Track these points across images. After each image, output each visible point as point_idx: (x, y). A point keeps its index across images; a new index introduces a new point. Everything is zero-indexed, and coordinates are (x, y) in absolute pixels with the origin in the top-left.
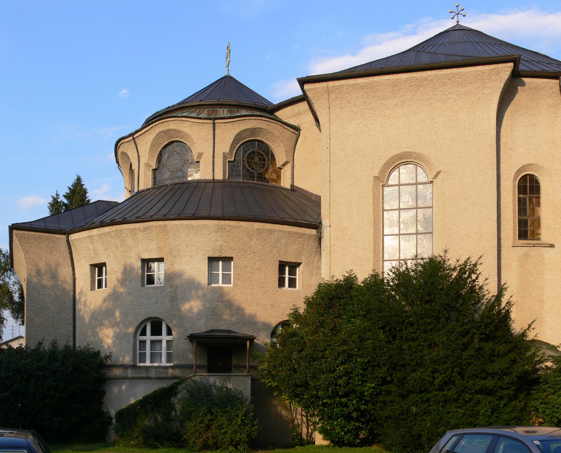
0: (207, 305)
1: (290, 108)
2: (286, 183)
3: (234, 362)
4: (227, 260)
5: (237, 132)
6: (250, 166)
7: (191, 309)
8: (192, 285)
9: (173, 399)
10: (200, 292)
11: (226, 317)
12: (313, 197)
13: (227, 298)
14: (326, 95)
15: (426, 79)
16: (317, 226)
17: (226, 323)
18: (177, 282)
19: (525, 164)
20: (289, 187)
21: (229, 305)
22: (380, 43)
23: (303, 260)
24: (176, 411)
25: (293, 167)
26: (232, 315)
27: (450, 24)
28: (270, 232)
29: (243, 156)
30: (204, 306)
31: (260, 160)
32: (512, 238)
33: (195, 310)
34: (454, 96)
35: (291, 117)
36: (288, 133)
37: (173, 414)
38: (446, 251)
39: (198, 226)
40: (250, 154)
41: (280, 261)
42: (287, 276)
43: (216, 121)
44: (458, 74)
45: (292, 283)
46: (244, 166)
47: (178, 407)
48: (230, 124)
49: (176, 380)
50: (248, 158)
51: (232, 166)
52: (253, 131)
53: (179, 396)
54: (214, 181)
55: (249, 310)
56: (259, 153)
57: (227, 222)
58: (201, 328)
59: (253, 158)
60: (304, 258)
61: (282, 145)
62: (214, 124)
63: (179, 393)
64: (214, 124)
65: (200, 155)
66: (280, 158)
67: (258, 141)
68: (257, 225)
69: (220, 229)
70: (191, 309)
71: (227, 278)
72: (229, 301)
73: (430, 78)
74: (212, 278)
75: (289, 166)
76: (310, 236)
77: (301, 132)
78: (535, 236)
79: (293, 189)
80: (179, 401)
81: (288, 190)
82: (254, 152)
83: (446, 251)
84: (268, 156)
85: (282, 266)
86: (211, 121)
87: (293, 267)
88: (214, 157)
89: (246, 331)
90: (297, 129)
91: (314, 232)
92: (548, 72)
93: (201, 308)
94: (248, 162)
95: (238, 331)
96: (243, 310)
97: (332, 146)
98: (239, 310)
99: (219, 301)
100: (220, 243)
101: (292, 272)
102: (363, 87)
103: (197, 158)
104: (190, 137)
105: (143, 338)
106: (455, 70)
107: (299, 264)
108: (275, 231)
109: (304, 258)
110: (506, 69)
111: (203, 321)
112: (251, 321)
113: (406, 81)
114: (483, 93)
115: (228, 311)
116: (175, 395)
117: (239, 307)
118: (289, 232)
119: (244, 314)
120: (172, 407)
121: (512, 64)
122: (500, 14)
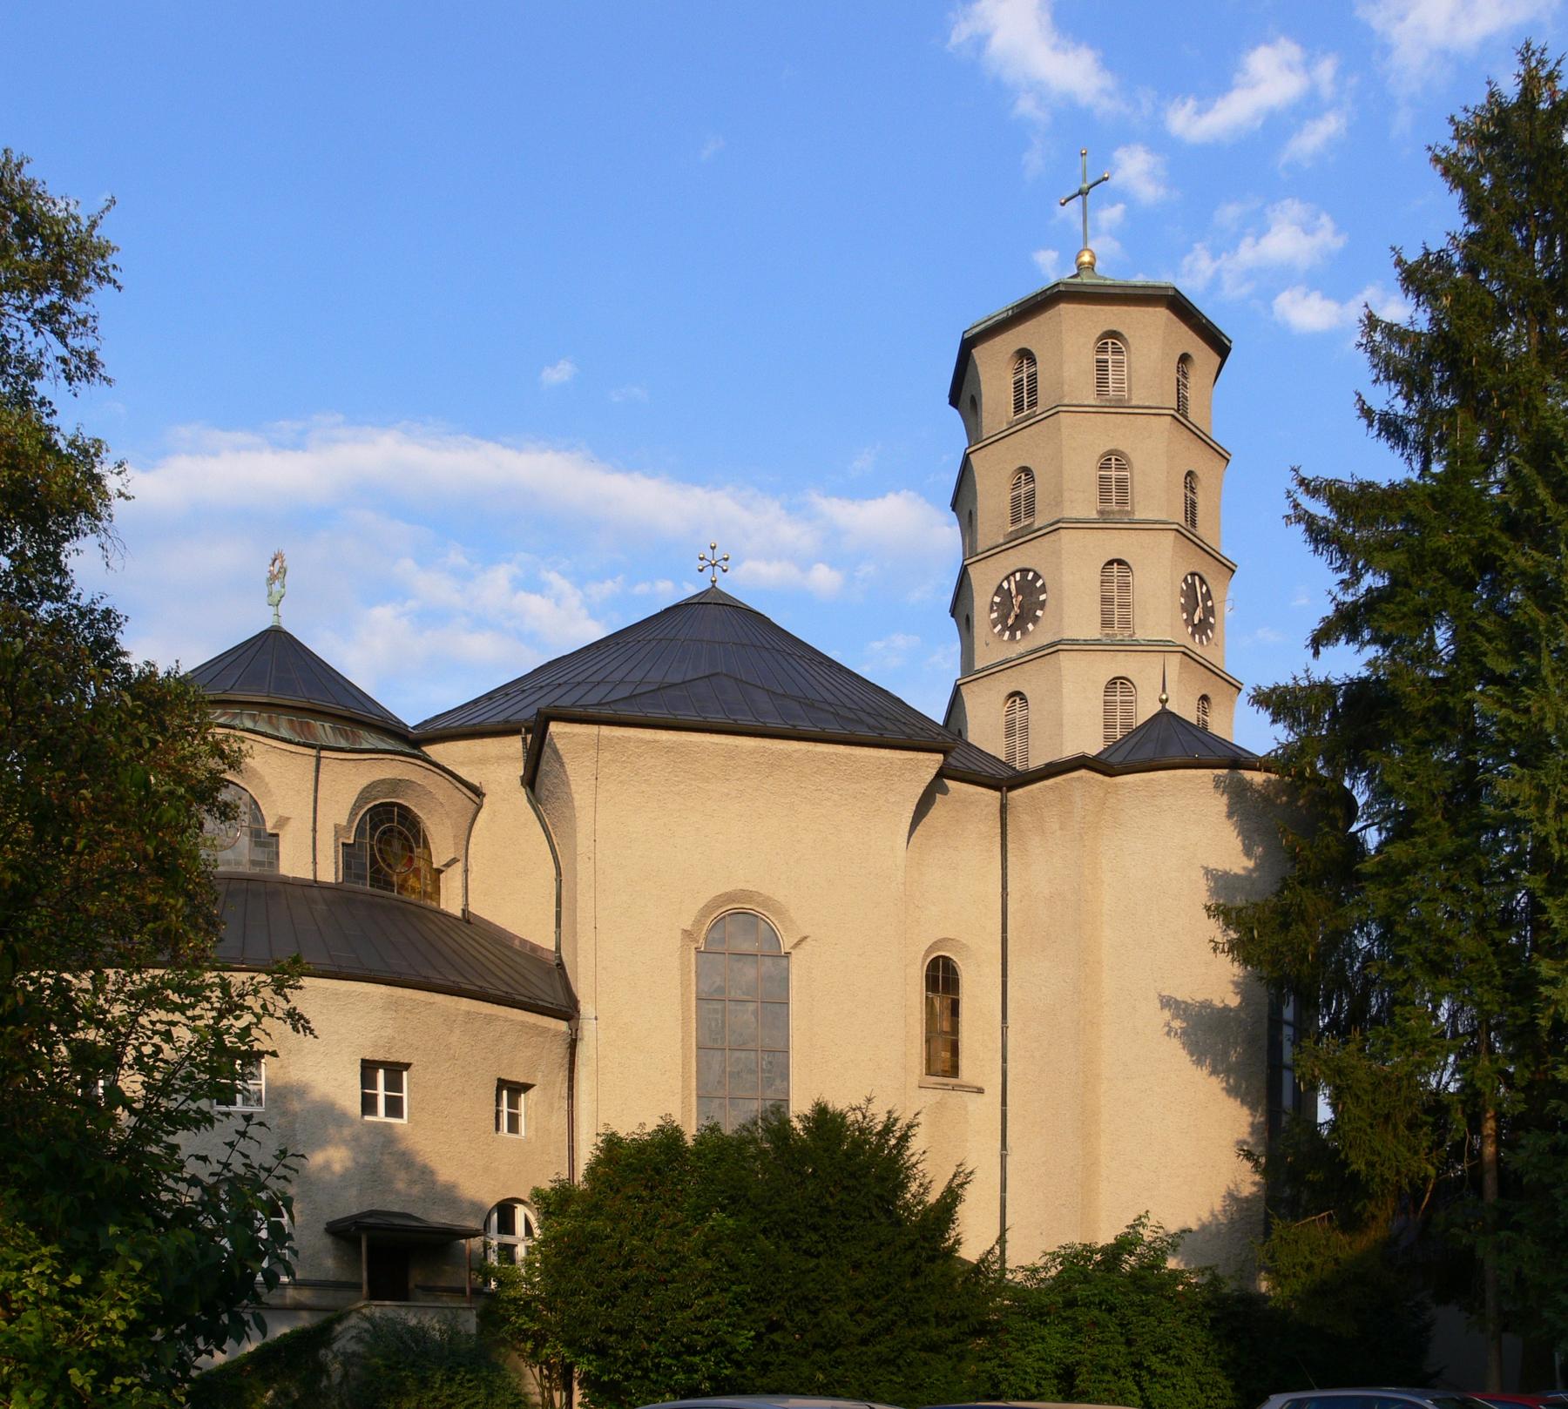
0: (362, 1159)
1: (462, 744)
2: (451, 902)
3: (416, 1277)
4: (395, 1071)
5: (365, 782)
6: (384, 860)
7: (327, 1166)
8: (328, 1114)
9: (322, 1352)
10: (346, 1132)
11: (400, 1186)
12: (517, 942)
13: (402, 1146)
14: (592, 752)
15: (789, 756)
16: (568, 1010)
17: (400, 1197)
18: (296, 1106)
19: (940, 936)
20: (459, 914)
21: (407, 1161)
22: (215, 453)
23: (538, 1079)
24: (329, 1377)
25: (466, 871)
26: (412, 1182)
27: (690, 590)
28: (489, 1019)
29: (372, 837)
30: (354, 1160)
31: (403, 848)
32: (917, 1071)
33: (337, 1167)
34: (836, 797)
35: (462, 764)
36: (462, 799)
37: (325, 1383)
38: (869, 1100)
39: (348, 994)
40: (384, 833)
41: (364, 1061)
42: (381, 1092)
43: (323, 753)
44: (847, 757)
45: (513, 1126)
46: (373, 856)
47: (336, 1368)
48: (351, 764)
49: (330, 1314)
50: (380, 841)
51: (349, 853)
52: (395, 785)
53: (335, 1347)
54: (315, 884)
55: (446, 1173)
56: (401, 833)
57: (408, 992)
58: (350, 1205)
59: (389, 843)
60: (540, 1075)
61: (448, 822)
62: (318, 759)
63: (335, 1339)
64: (318, 759)
65: (283, 821)
66: (441, 848)
67: (400, 806)
68: (465, 1004)
69: (395, 1005)
70: (327, 1166)
71: (394, 1107)
72: (404, 1154)
73: (796, 755)
74: (368, 1104)
75: (459, 866)
76: (556, 1034)
77: (485, 800)
78: (954, 1070)
79: (467, 918)
80: (335, 1357)
81: (456, 918)
82: (391, 830)
83: (869, 1100)
84: (417, 843)
85: (502, 1084)
86: (314, 752)
87: (395, 1071)
88: (314, 830)
89: (439, 1217)
90: (477, 792)
91: (563, 1026)
92: (979, 774)
93: (349, 1164)
94: (380, 850)
95: (424, 1217)
96: (432, 1173)
97: (599, 856)
98: (426, 1173)
99: (385, 1154)
100: (389, 1032)
101: (394, 1083)
102: (669, 749)
103: (275, 827)
104: (261, 778)
105: (508, 1239)
106: (841, 749)
107: (526, 1087)
108: (498, 1018)
109: (540, 1075)
110: (930, 763)
111: (354, 1191)
112: (448, 1197)
113: (752, 752)
114: (887, 801)
115: (402, 1175)
116: (328, 1344)
117: (425, 1166)
118: (523, 1024)
119: (434, 1183)
120: (321, 1369)
121: (940, 757)
122: (506, 446)
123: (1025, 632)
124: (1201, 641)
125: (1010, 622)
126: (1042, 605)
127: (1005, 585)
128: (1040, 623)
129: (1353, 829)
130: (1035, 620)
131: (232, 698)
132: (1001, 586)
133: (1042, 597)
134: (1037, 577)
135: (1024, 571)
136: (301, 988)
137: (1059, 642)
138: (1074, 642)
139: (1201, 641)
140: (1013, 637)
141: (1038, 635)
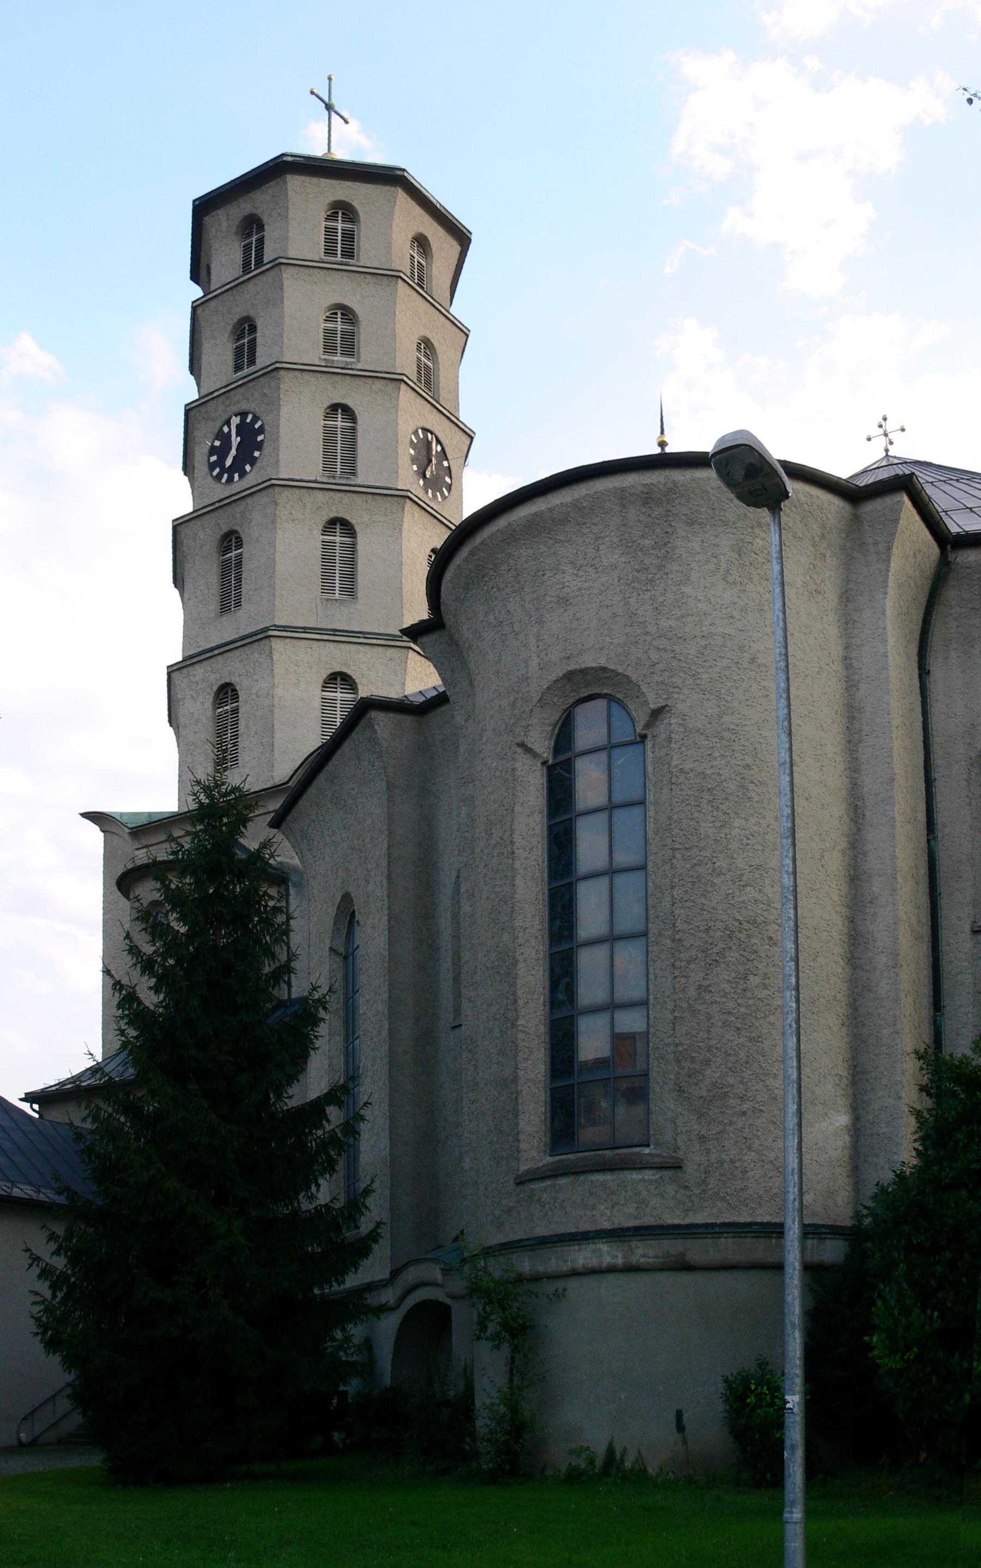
16: (472, 438)
123: (243, 474)
124: (435, 496)
125: (229, 462)
126: (259, 446)
127: (226, 429)
128: (258, 464)
129: (37, 1116)
130: (253, 461)
131: (518, 1234)
132: (221, 429)
133: (260, 438)
134: (256, 418)
135: (243, 415)
136: (358, 947)
137: (267, 629)
138: (285, 628)
139: (435, 496)
140: (230, 480)
141: (253, 476)
